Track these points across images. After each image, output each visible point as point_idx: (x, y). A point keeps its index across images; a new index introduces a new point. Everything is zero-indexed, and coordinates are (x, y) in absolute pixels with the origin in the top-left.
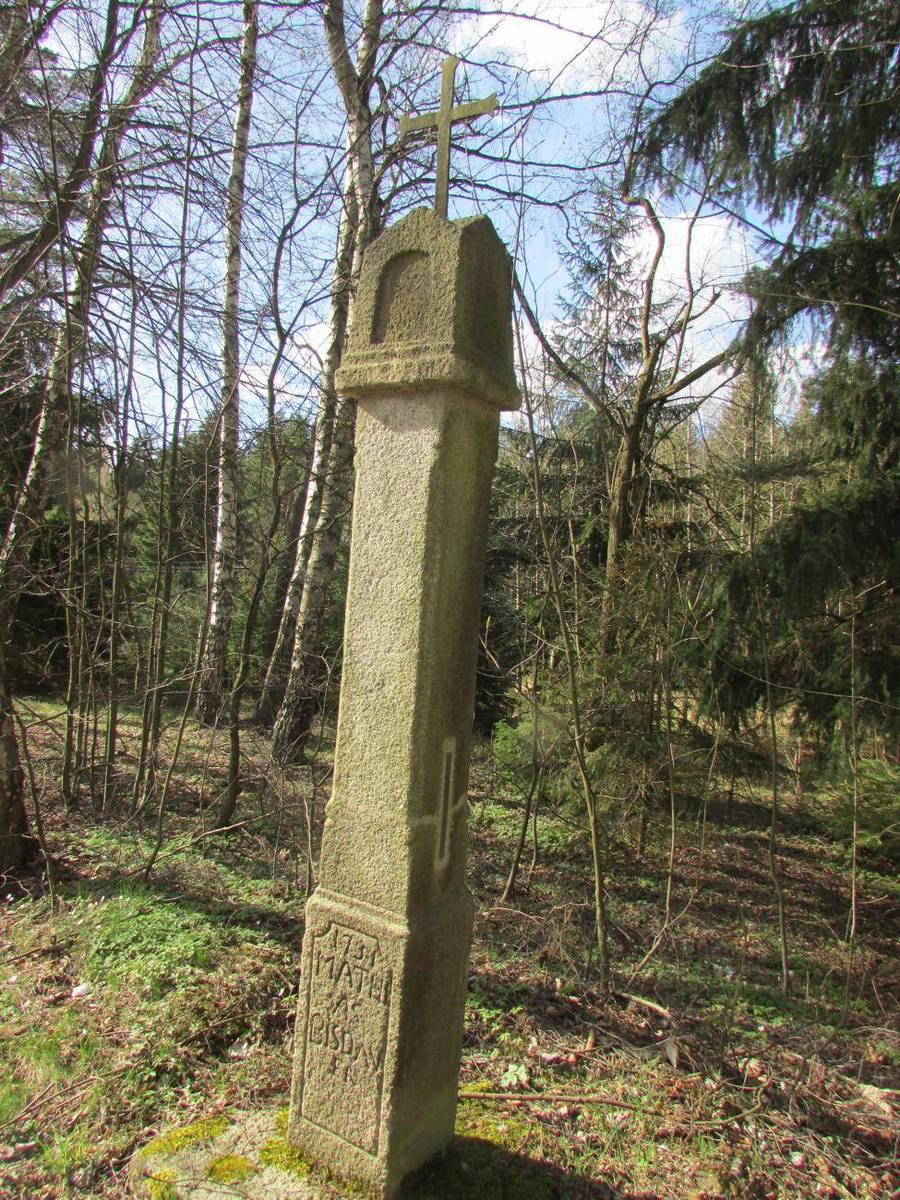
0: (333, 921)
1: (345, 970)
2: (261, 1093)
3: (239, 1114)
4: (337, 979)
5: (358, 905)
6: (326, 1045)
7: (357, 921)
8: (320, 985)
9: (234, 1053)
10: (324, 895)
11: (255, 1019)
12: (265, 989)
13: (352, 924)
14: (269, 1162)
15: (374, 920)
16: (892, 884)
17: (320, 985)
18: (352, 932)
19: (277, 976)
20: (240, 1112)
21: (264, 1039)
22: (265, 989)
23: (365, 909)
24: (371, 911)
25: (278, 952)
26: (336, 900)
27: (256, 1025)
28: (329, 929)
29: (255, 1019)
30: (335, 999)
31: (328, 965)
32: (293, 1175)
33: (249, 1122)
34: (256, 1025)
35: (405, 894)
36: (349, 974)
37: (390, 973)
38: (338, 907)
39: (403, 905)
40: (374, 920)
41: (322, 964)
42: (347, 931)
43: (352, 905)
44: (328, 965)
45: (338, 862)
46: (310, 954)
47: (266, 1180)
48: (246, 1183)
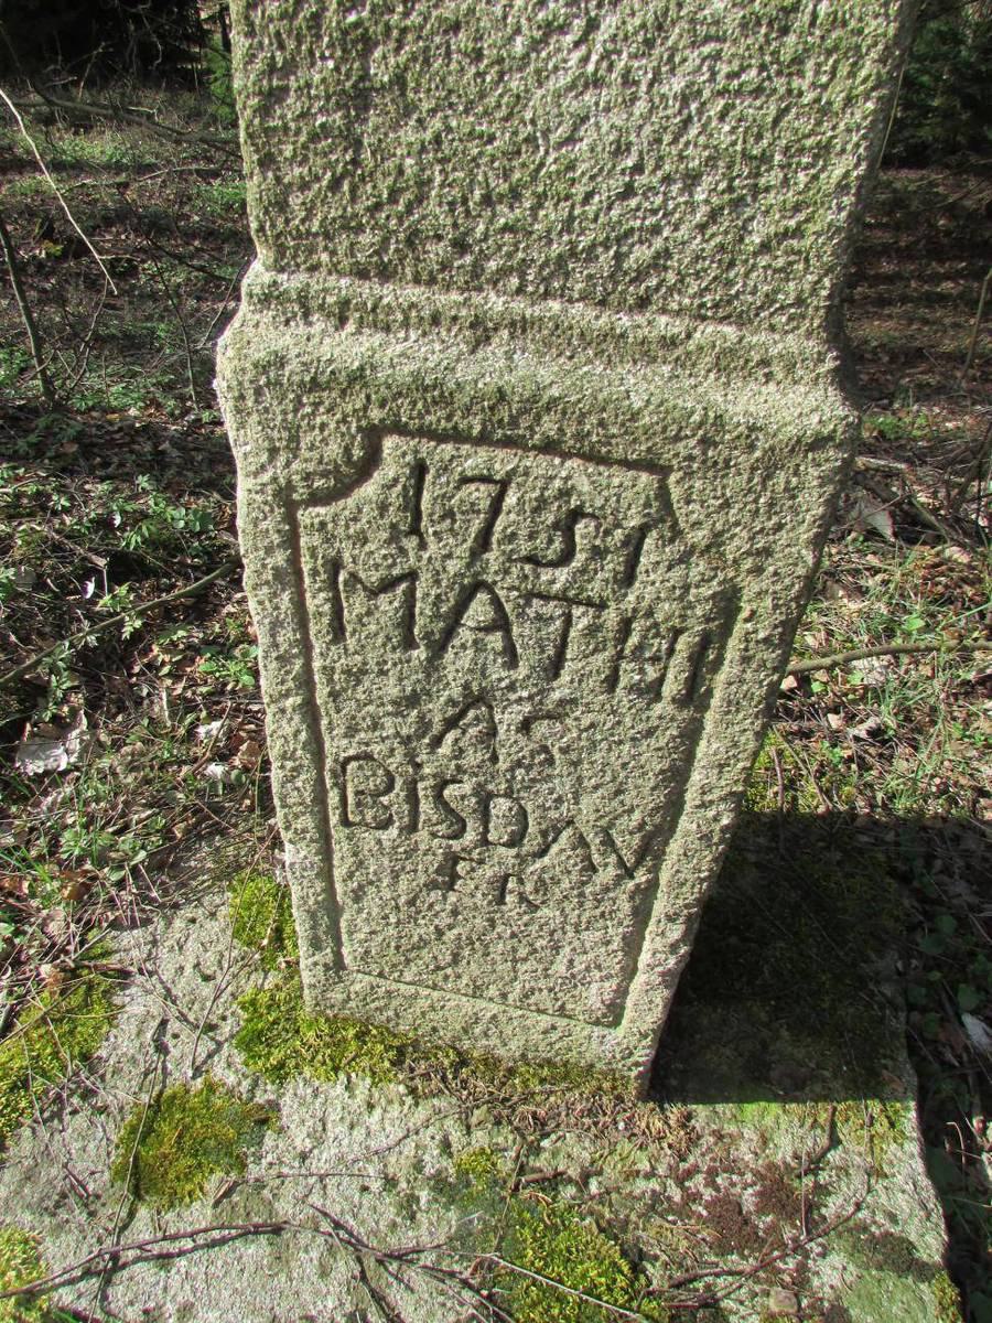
0: (380, 424)
1: (479, 610)
2: (158, 863)
3: (130, 945)
4: (438, 647)
5: (520, 326)
6: (412, 827)
7: (535, 405)
8: (356, 675)
9: (34, 767)
10: (305, 305)
11: (53, 670)
12: (40, 585)
13: (507, 422)
14: (279, 1073)
15: (639, 386)
16: (980, 193)
17: (356, 675)
18: (503, 461)
19: (57, 548)
20: (128, 938)
21: (93, 705)
22: (40, 585)
23: (558, 337)
24: (607, 344)
25: (31, 489)
26: (377, 319)
27: (61, 683)
28: (372, 459)
29: (53, 670)
30: (436, 710)
31: (389, 605)
32: (363, 1086)
33: (167, 965)
34: (61, 683)
35: (834, 215)
36: (501, 623)
37: (727, 605)
38: (402, 355)
39: (815, 282)
40: (639, 386)
41: (355, 606)
42: (475, 460)
43: (481, 331)
44: (389, 605)
45: (359, 98)
46: (290, 576)
47: (301, 1141)
48: (254, 1171)
